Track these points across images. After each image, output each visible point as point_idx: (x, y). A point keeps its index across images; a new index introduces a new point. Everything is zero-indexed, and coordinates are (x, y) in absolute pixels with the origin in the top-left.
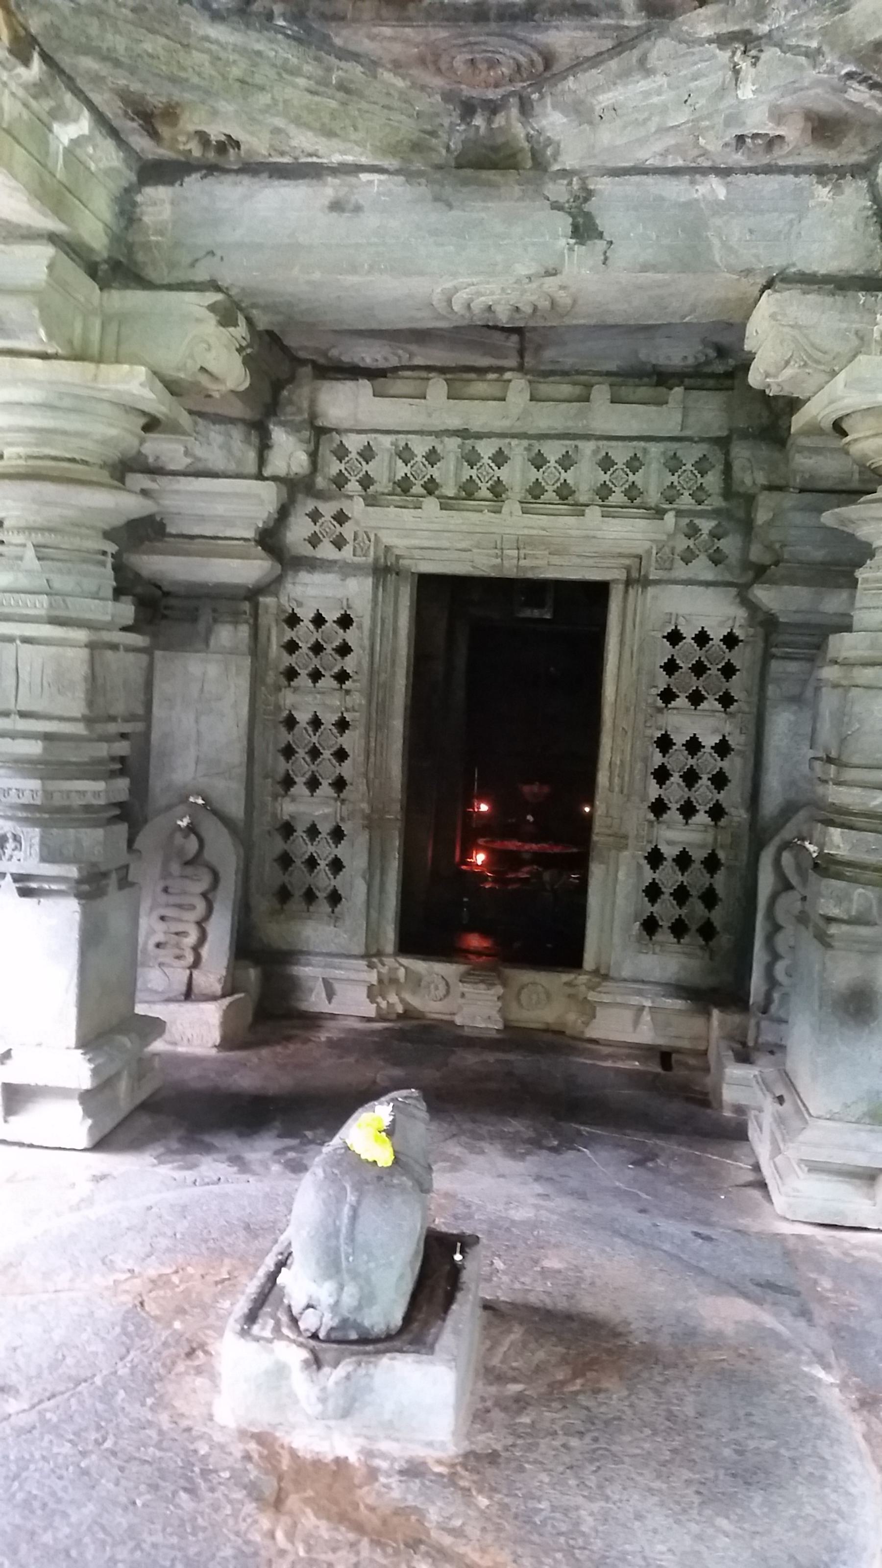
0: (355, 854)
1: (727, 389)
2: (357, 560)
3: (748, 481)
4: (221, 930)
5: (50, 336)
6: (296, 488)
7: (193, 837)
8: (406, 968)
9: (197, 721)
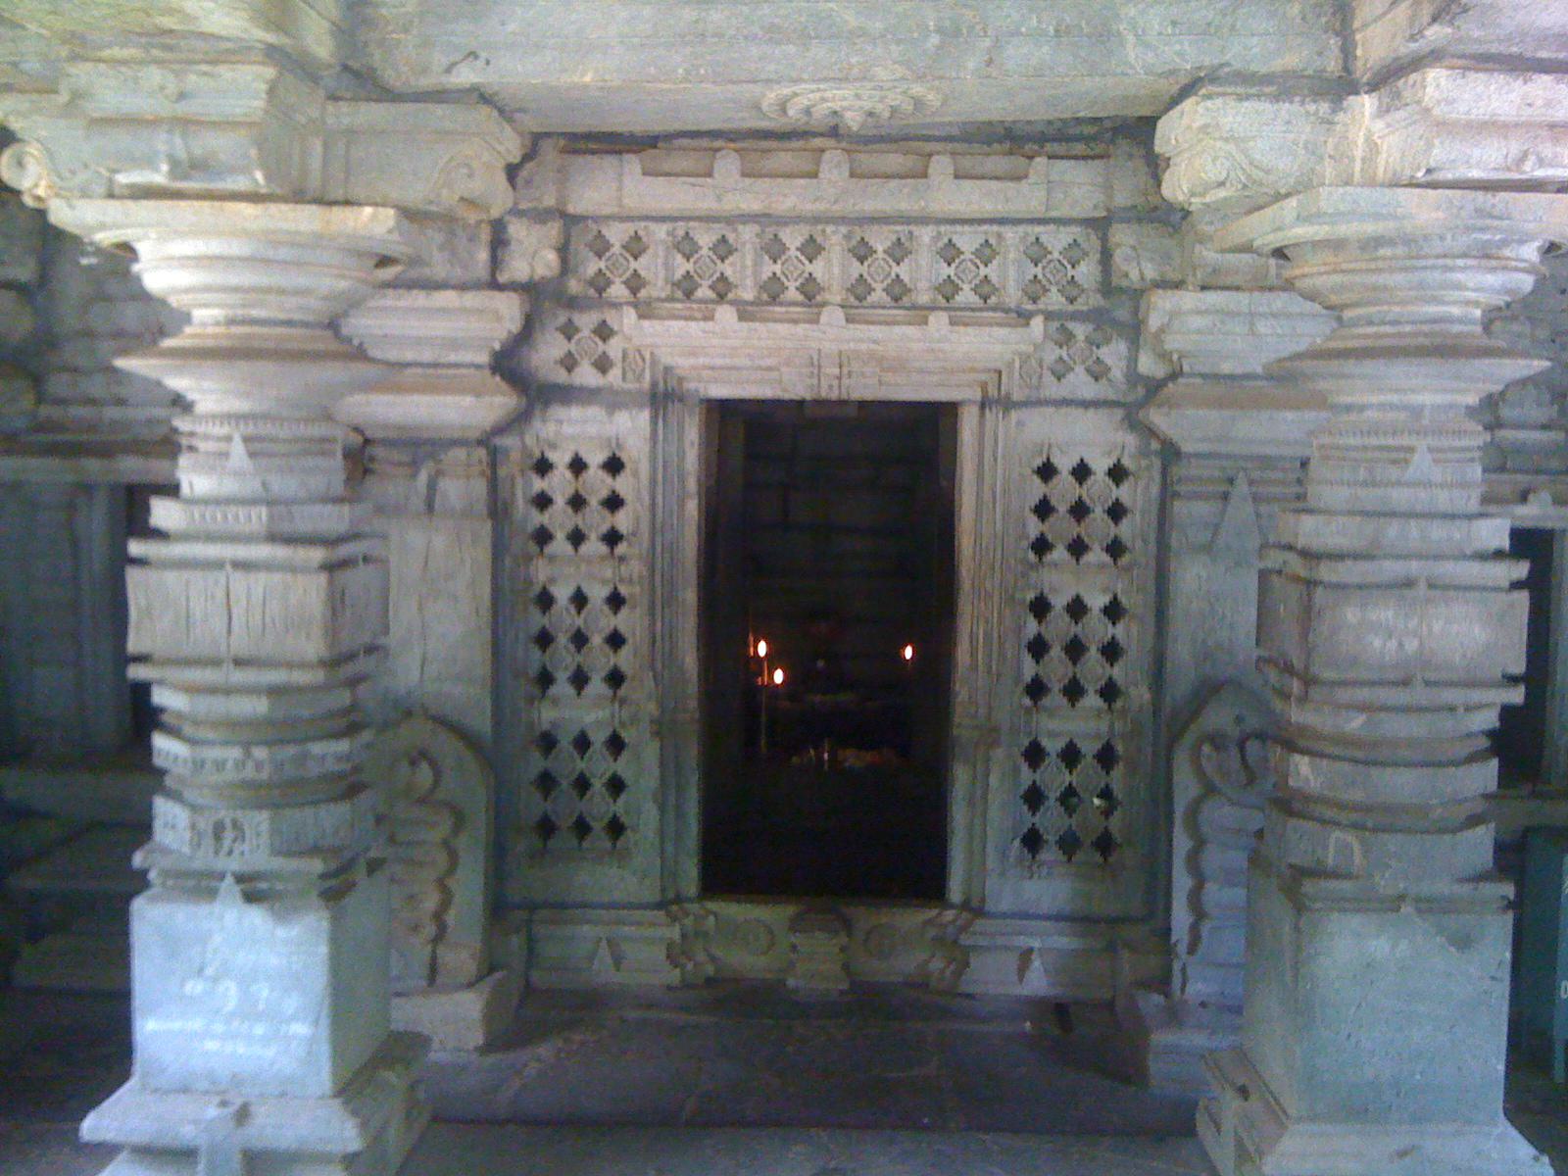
0: (642, 768)
1: (1101, 157)
2: (630, 386)
3: (1134, 275)
4: (470, 886)
5: (268, 178)
6: (542, 299)
7: (424, 766)
8: (716, 915)
9: (421, 608)
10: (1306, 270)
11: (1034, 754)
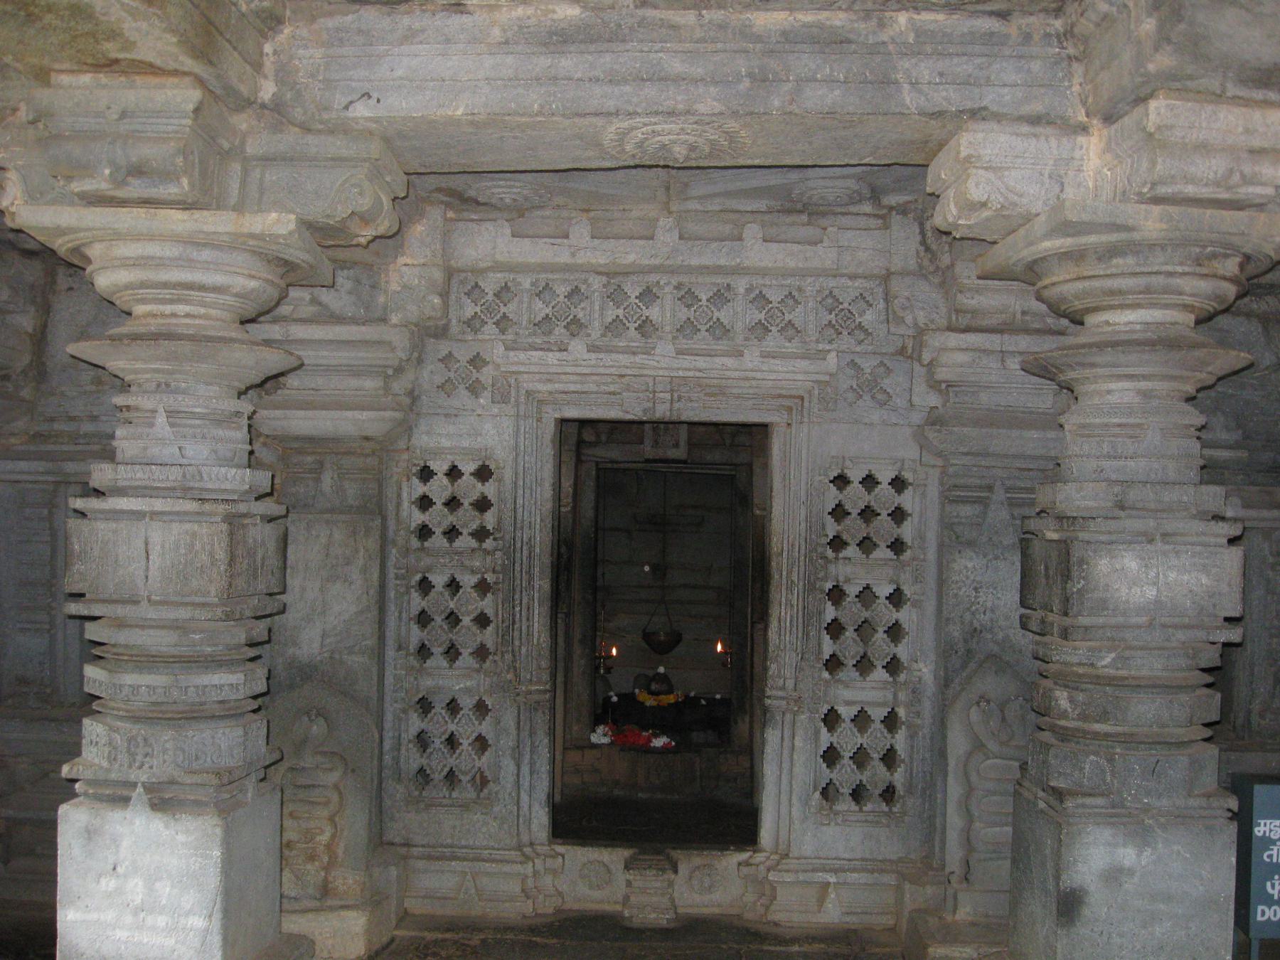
0: (503, 727)
10: (1055, 279)
11: (831, 719)
